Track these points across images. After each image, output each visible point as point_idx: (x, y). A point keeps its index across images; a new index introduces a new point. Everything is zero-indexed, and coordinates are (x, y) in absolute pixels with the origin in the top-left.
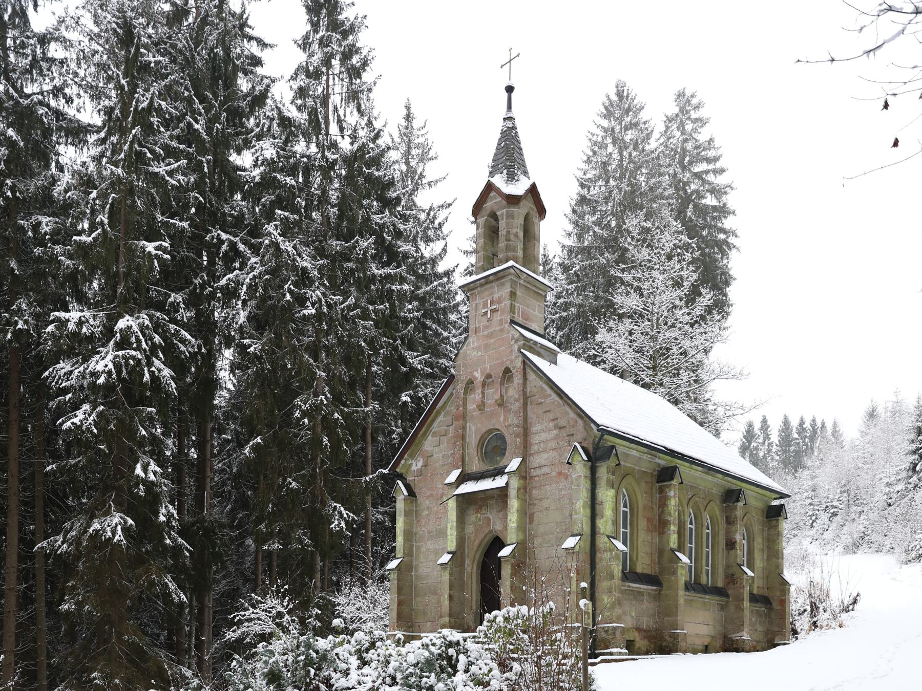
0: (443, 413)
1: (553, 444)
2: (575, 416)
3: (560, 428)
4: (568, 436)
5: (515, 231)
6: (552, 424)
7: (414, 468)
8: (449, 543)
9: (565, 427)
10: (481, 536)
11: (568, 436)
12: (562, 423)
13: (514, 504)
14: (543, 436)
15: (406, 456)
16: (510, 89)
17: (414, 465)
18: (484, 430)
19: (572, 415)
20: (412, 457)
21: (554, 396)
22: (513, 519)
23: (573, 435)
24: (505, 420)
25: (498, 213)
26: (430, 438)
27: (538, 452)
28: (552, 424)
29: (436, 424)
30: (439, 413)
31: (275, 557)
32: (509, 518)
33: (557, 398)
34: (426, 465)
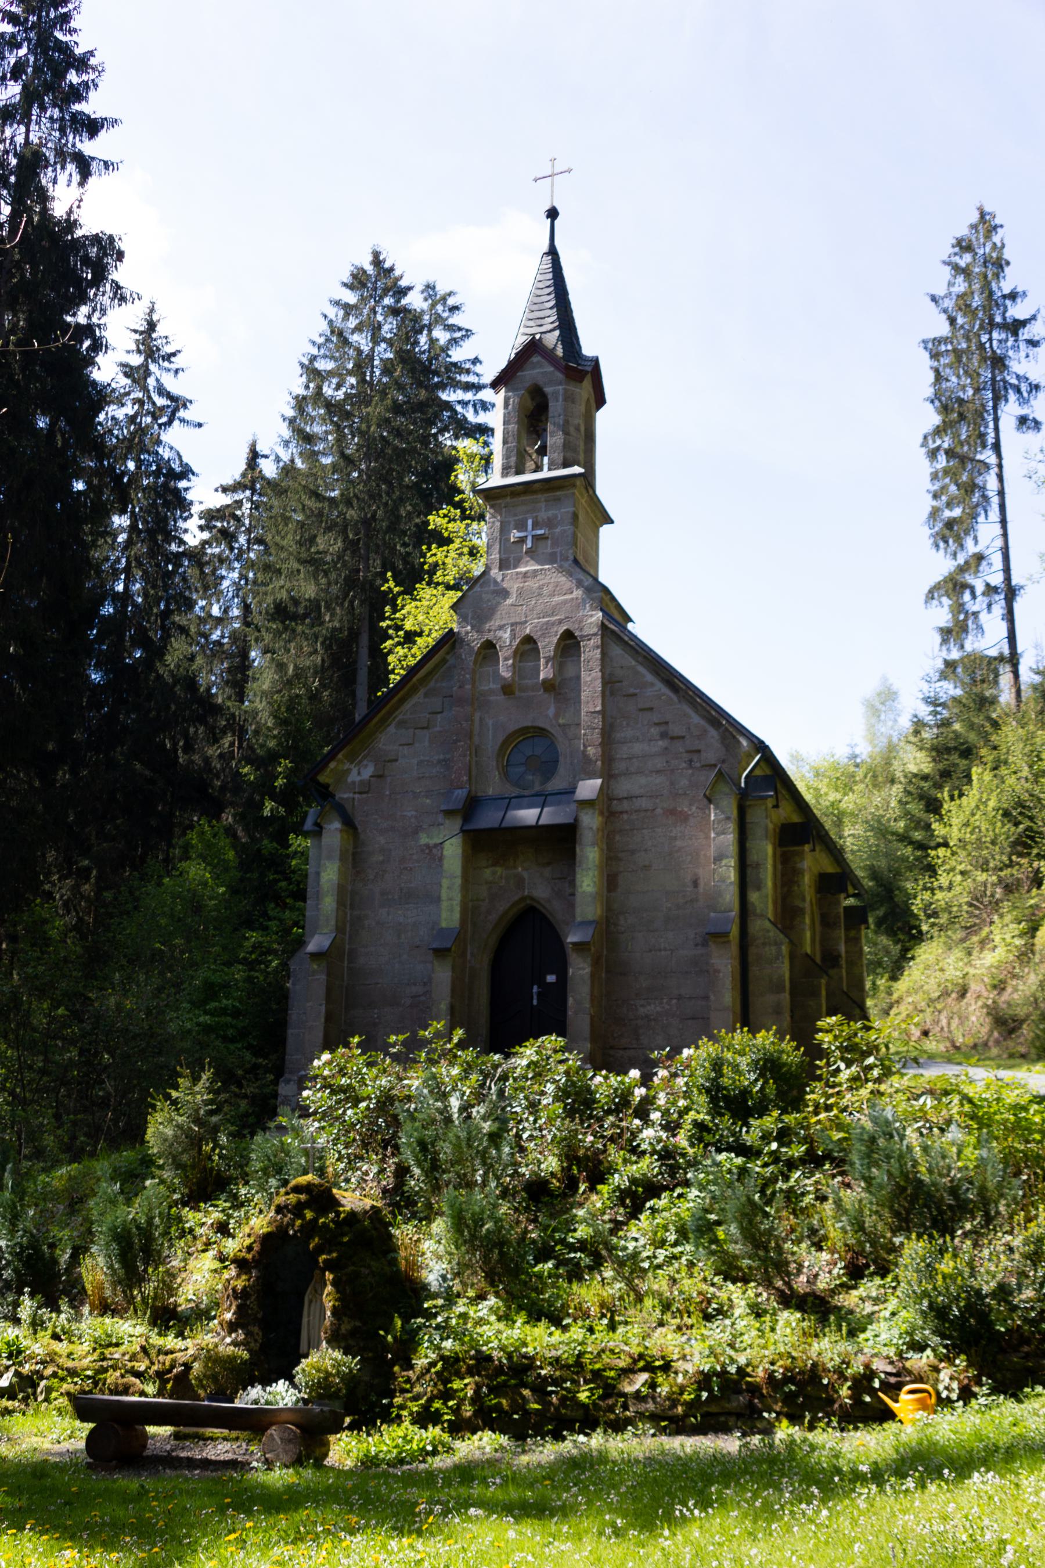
0: (422, 691)
1: (659, 763)
2: (702, 722)
3: (672, 738)
4: (688, 752)
5: (576, 422)
6: (654, 731)
7: (353, 777)
8: (444, 915)
9: (683, 737)
10: (502, 906)
11: (688, 752)
12: (676, 730)
13: (590, 855)
14: (638, 748)
15: (340, 756)
16: (553, 214)
17: (355, 771)
18: (513, 727)
19: (696, 719)
20: (352, 758)
21: (660, 686)
22: (588, 882)
23: (699, 751)
24: (557, 715)
25: (548, 390)
26: (392, 729)
27: (627, 773)
28: (654, 731)
29: (408, 706)
30: (415, 690)
31: (728, 996)
32: (917, 906)
33: (665, 690)
34: (379, 776)
